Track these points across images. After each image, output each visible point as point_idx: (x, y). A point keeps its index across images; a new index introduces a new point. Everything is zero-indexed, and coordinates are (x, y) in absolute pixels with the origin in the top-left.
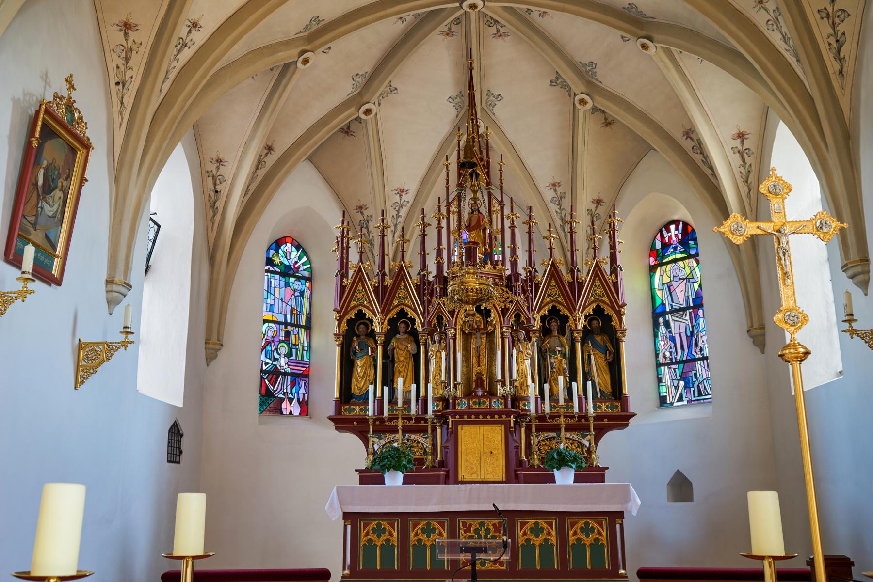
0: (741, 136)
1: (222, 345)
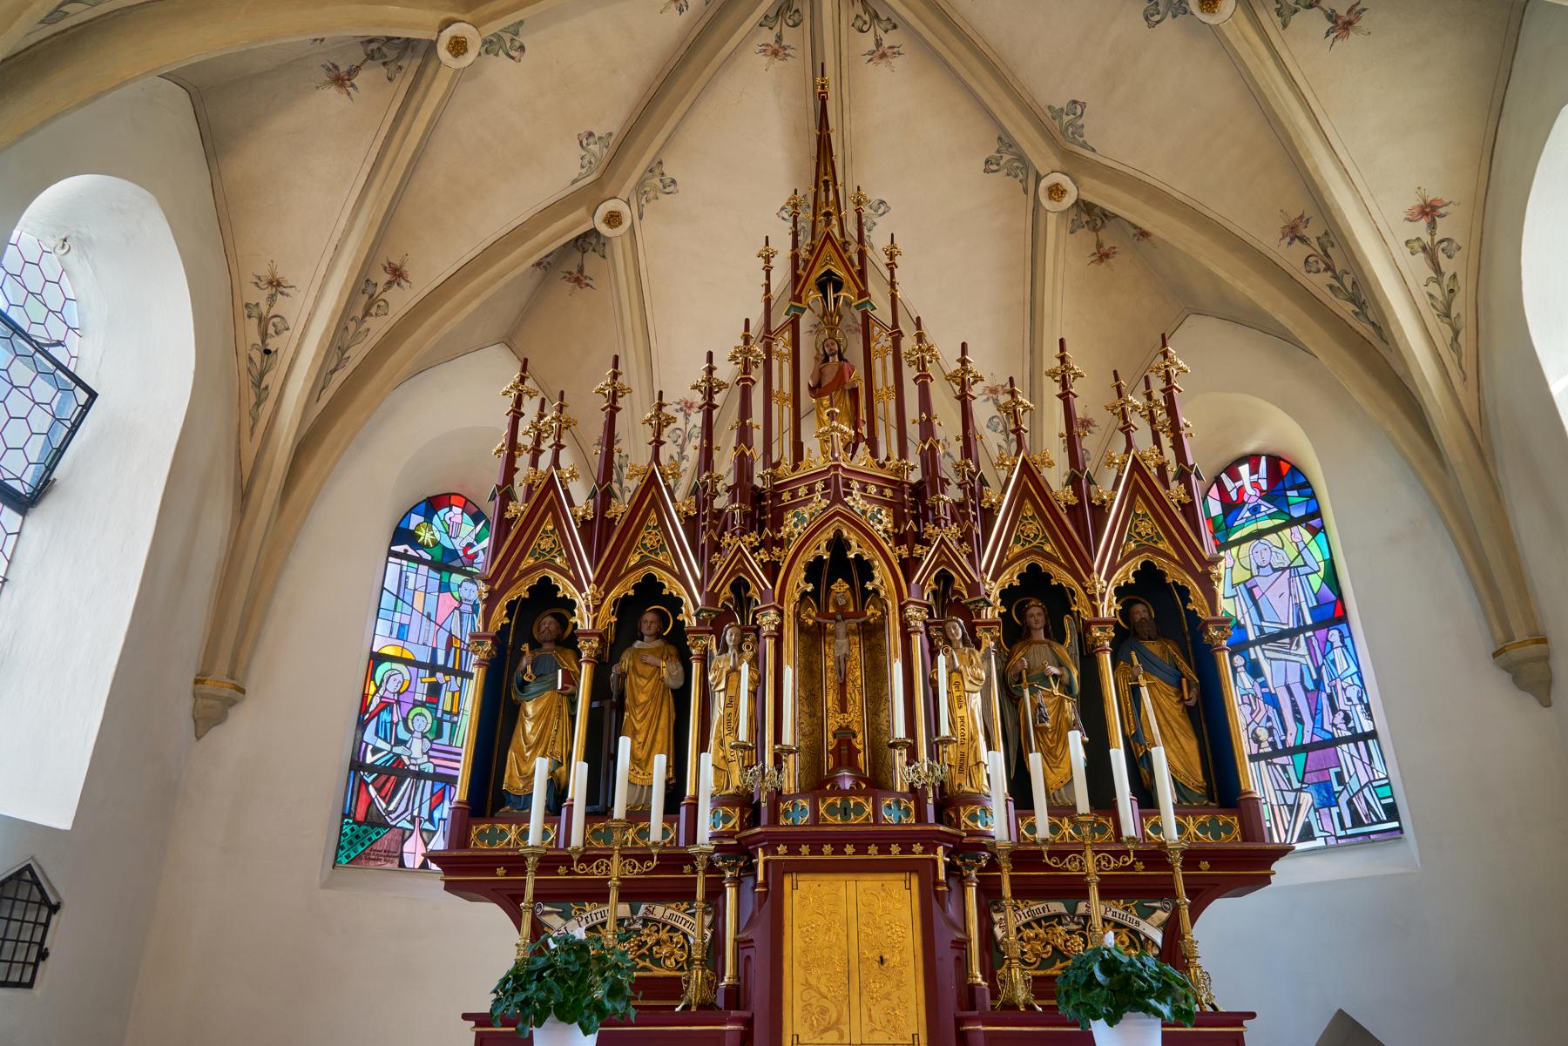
0: (1429, 211)
1: (243, 691)
